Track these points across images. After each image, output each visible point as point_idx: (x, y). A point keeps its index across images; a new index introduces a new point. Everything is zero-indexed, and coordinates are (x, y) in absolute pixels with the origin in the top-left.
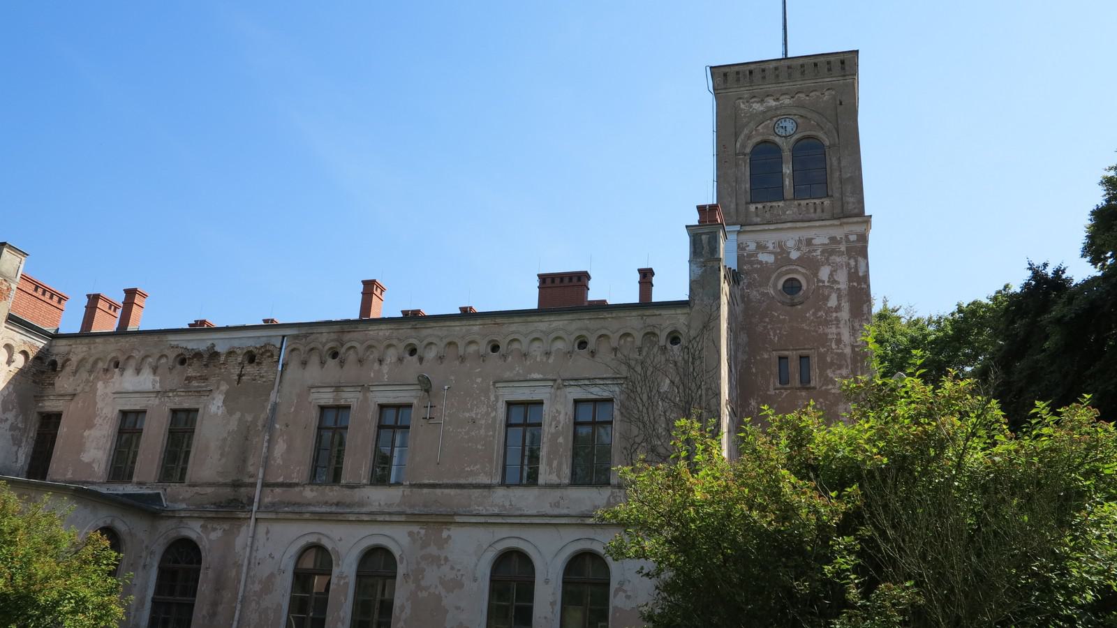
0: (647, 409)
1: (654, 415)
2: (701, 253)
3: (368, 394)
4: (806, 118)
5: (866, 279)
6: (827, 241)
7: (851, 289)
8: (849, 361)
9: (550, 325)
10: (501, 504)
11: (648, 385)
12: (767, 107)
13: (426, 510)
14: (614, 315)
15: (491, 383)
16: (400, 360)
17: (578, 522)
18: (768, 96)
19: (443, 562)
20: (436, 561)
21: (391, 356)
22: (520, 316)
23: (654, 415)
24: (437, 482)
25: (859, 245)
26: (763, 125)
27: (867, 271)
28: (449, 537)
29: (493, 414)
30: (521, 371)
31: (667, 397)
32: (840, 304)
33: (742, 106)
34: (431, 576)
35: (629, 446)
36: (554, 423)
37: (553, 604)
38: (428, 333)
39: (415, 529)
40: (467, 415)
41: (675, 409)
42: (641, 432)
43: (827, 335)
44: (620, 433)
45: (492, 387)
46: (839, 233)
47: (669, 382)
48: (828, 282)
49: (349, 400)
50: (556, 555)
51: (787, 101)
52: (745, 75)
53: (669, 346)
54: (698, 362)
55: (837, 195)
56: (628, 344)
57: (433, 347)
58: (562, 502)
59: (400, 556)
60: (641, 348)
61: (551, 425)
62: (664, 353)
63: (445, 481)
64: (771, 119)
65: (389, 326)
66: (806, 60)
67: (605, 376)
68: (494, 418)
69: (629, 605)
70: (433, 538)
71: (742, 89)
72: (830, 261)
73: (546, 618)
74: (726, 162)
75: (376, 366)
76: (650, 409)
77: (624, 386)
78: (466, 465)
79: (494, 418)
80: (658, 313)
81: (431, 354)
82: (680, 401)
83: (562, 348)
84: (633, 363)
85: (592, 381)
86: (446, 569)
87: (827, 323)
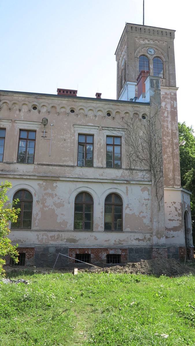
0: (135, 141)
1: (137, 144)
2: (153, 87)
3: (14, 124)
4: (158, 50)
5: (176, 108)
6: (164, 94)
7: (171, 111)
8: (170, 135)
9: (96, 105)
10: (79, 174)
11: (135, 133)
12: (145, 43)
13: (45, 174)
14: (122, 104)
15: (72, 125)
16: (30, 111)
17: (111, 182)
18: (146, 39)
19: (54, 196)
20: (52, 195)
21: (25, 109)
22: (85, 100)
23: (137, 144)
24: (49, 163)
25: (175, 97)
26: (143, 49)
27: (177, 106)
28: (57, 186)
29: (73, 138)
30: (84, 122)
31: (142, 138)
32: (168, 116)
33: (137, 40)
34: (49, 202)
35: (129, 155)
36: (99, 144)
37: (102, 212)
38: (43, 101)
39: (41, 182)
40: (62, 137)
41: (145, 143)
42: (133, 150)
43: (164, 125)
44: (126, 150)
45: (72, 127)
46: (168, 92)
47: (143, 132)
48: (164, 107)
49: (4, 125)
50: (103, 194)
51: (152, 42)
52: (138, 29)
53: (142, 119)
54: (154, 126)
55: (167, 78)
56: (127, 117)
57: (45, 107)
58: (104, 174)
59: (35, 193)
60: (132, 118)
61: (98, 144)
62: (140, 122)
63: (53, 163)
64: (146, 47)
65: (24, 95)
66: (159, 29)
67: (118, 127)
68: (74, 139)
69: (131, 213)
70: (49, 186)
71: (137, 34)
72: (165, 101)
73: (99, 218)
74: (131, 59)
75: (18, 112)
76: (136, 142)
77: (126, 132)
78: (62, 157)
79: (74, 139)
80: (139, 106)
81: (44, 110)
82: (147, 140)
83: (101, 115)
84: (129, 124)
85: (114, 129)
86: (56, 199)
87: (164, 121)
